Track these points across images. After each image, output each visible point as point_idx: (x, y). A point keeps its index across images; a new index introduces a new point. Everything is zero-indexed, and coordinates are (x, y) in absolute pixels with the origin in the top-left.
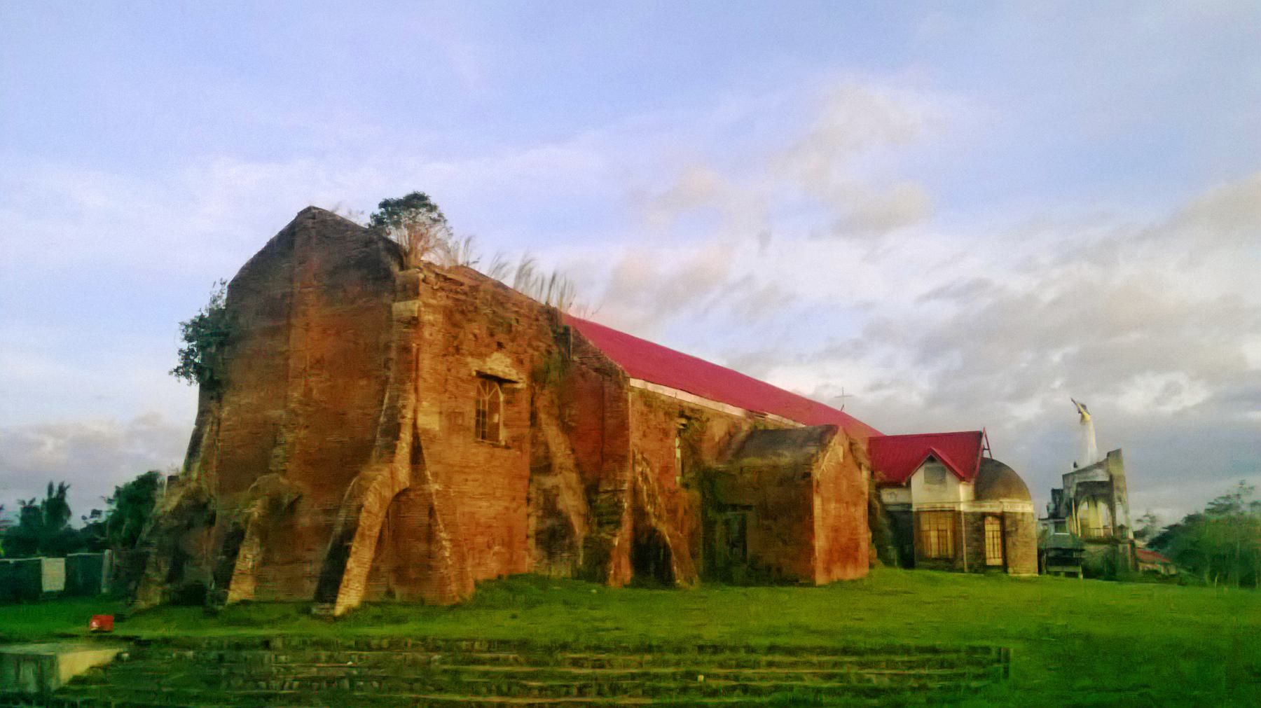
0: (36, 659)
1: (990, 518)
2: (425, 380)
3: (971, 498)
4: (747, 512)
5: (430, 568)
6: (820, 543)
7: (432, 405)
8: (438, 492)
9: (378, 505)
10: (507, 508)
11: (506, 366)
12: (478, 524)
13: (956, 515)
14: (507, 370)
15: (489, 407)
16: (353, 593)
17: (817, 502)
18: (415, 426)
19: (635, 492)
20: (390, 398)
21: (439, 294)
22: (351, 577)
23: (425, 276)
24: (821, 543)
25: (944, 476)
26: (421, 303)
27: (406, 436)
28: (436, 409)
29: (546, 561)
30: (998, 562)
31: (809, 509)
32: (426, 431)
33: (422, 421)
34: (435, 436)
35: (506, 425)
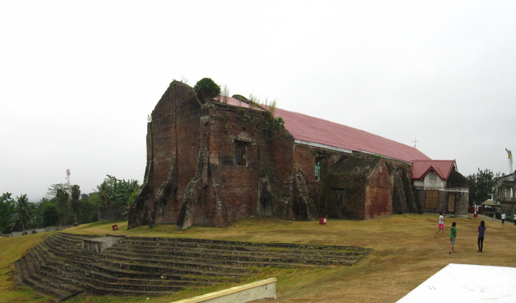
0: (98, 243)
1: (451, 194)
2: (212, 146)
3: (445, 186)
4: (343, 191)
5: (215, 213)
6: (368, 203)
7: (215, 155)
8: (217, 187)
9: (196, 192)
10: (248, 190)
11: (247, 137)
12: (236, 197)
13: (439, 192)
14: (247, 138)
15: (245, 149)
16: (189, 222)
17: (368, 188)
18: (209, 163)
19: (294, 184)
20: (201, 153)
21: (217, 112)
22: (187, 217)
23: (210, 106)
24: (368, 204)
25: (436, 176)
26: (209, 116)
27: (206, 167)
28: (217, 156)
29: (263, 209)
30: (452, 210)
31: (364, 191)
32: (213, 165)
33: (211, 161)
34: (217, 166)
35: (248, 160)
